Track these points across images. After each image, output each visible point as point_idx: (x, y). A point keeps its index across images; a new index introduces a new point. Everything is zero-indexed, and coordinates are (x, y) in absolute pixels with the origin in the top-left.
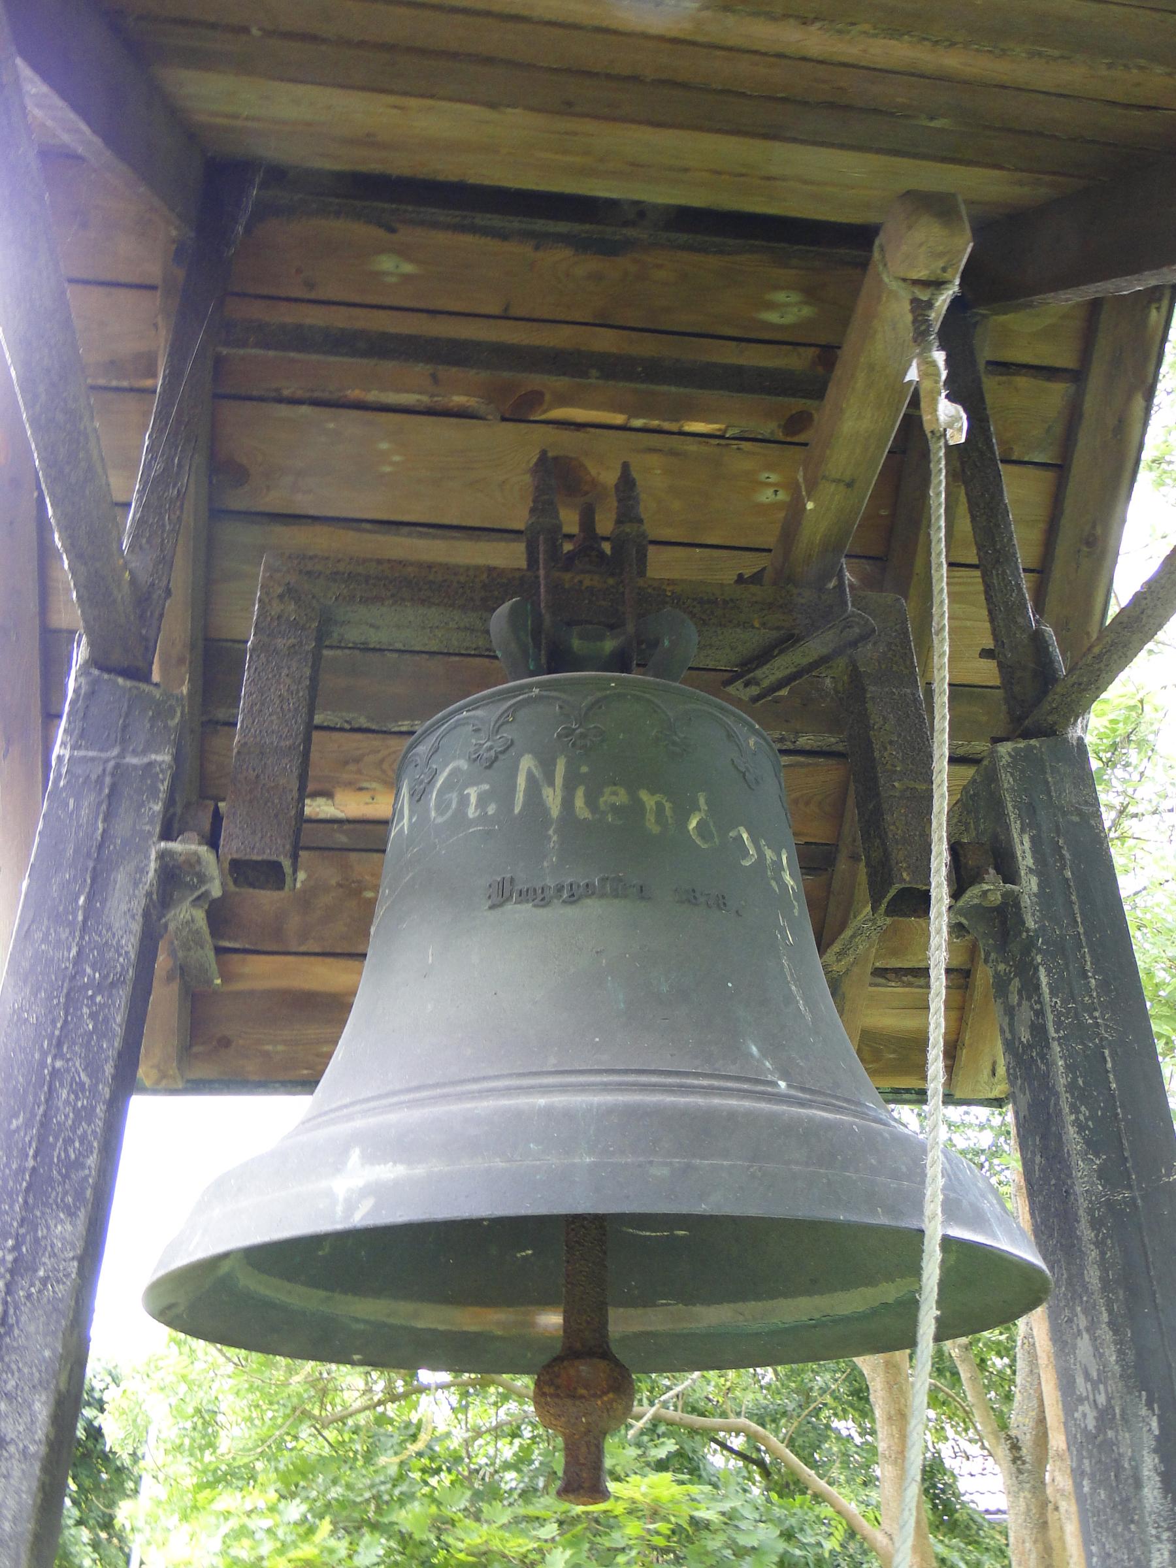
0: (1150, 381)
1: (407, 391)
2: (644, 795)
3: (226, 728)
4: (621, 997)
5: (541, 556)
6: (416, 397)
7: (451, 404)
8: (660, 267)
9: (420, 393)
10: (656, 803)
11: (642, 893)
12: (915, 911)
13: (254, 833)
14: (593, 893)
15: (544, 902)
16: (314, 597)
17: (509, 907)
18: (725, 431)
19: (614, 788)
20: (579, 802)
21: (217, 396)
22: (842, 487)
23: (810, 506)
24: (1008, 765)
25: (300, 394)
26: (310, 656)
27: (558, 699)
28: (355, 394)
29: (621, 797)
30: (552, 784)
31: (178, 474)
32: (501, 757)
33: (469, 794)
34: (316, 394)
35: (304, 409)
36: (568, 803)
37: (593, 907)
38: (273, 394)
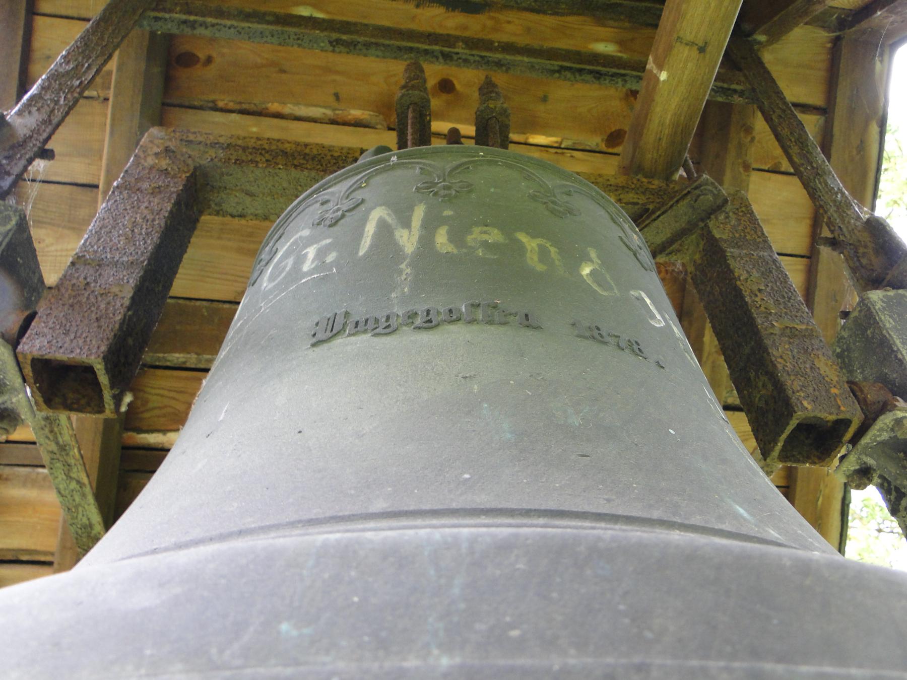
0: (881, 113)
1: (315, 106)
2: (523, 237)
3: (152, 370)
4: (506, 426)
6: (323, 110)
7: (350, 117)
8: (509, 22)
9: (325, 107)
10: (539, 246)
11: (528, 322)
12: (808, 458)
14: (458, 320)
15: (390, 330)
17: (339, 341)
18: (561, 143)
19: (485, 229)
20: (441, 238)
21: (164, 104)
22: (695, 53)
23: (663, 76)
25: (231, 106)
26: (174, 196)
27: (418, 163)
28: (275, 107)
29: (495, 236)
30: (407, 224)
31: (85, 72)
32: (347, 214)
33: (306, 254)
34: (244, 106)
35: (234, 116)
36: (426, 240)
37: (457, 334)
38: (211, 105)
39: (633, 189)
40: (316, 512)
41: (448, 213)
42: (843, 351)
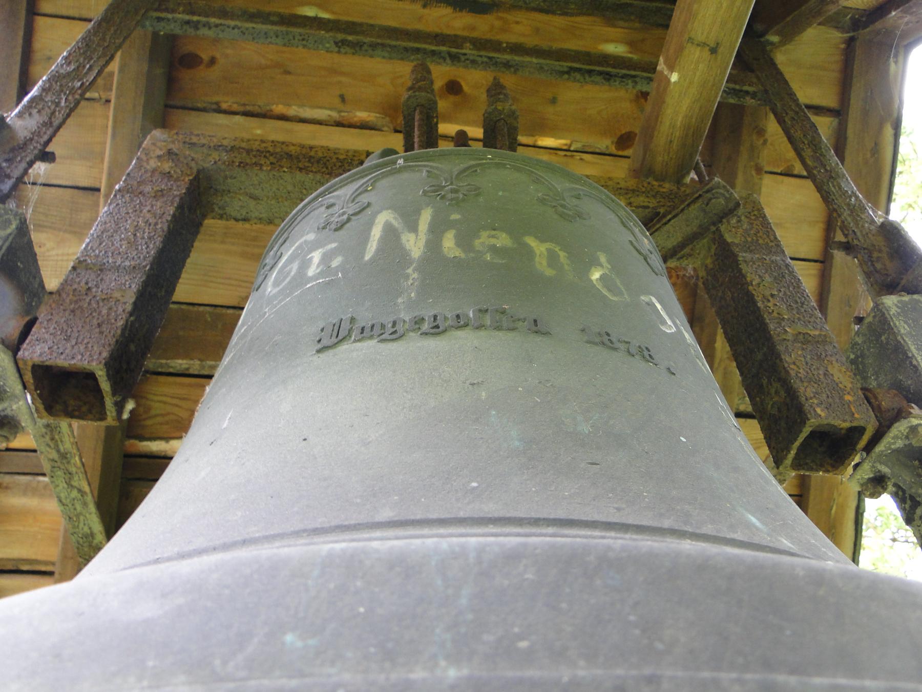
0: (895, 115)
1: (321, 108)
2: (531, 241)
3: (155, 377)
4: (514, 433)
5: (416, 124)
6: (328, 112)
7: (355, 119)
8: (517, 23)
9: (331, 109)
10: (548, 250)
11: (536, 327)
12: (822, 466)
13: (68, 339)
14: (466, 325)
15: (396, 336)
16: (193, 160)
17: (344, 347)
18: (570, 146)
19: (493, 233)
20: (449, 242)
21: (166, 106)
22: (706, 54)
23: (674, 77)
24: (898, 313)
25: (235, 107)
26: (177, 199)
27: (425, 166)
28: (279, 109)
29: (503, 240)
30: (414, 228)
31: (87, 73)
32: (353, 218)
33: (311, 258)
34: (248, 108)
35: (238, 118)
36: (433, 244)
37: (465, 340)
40: (321, 521)
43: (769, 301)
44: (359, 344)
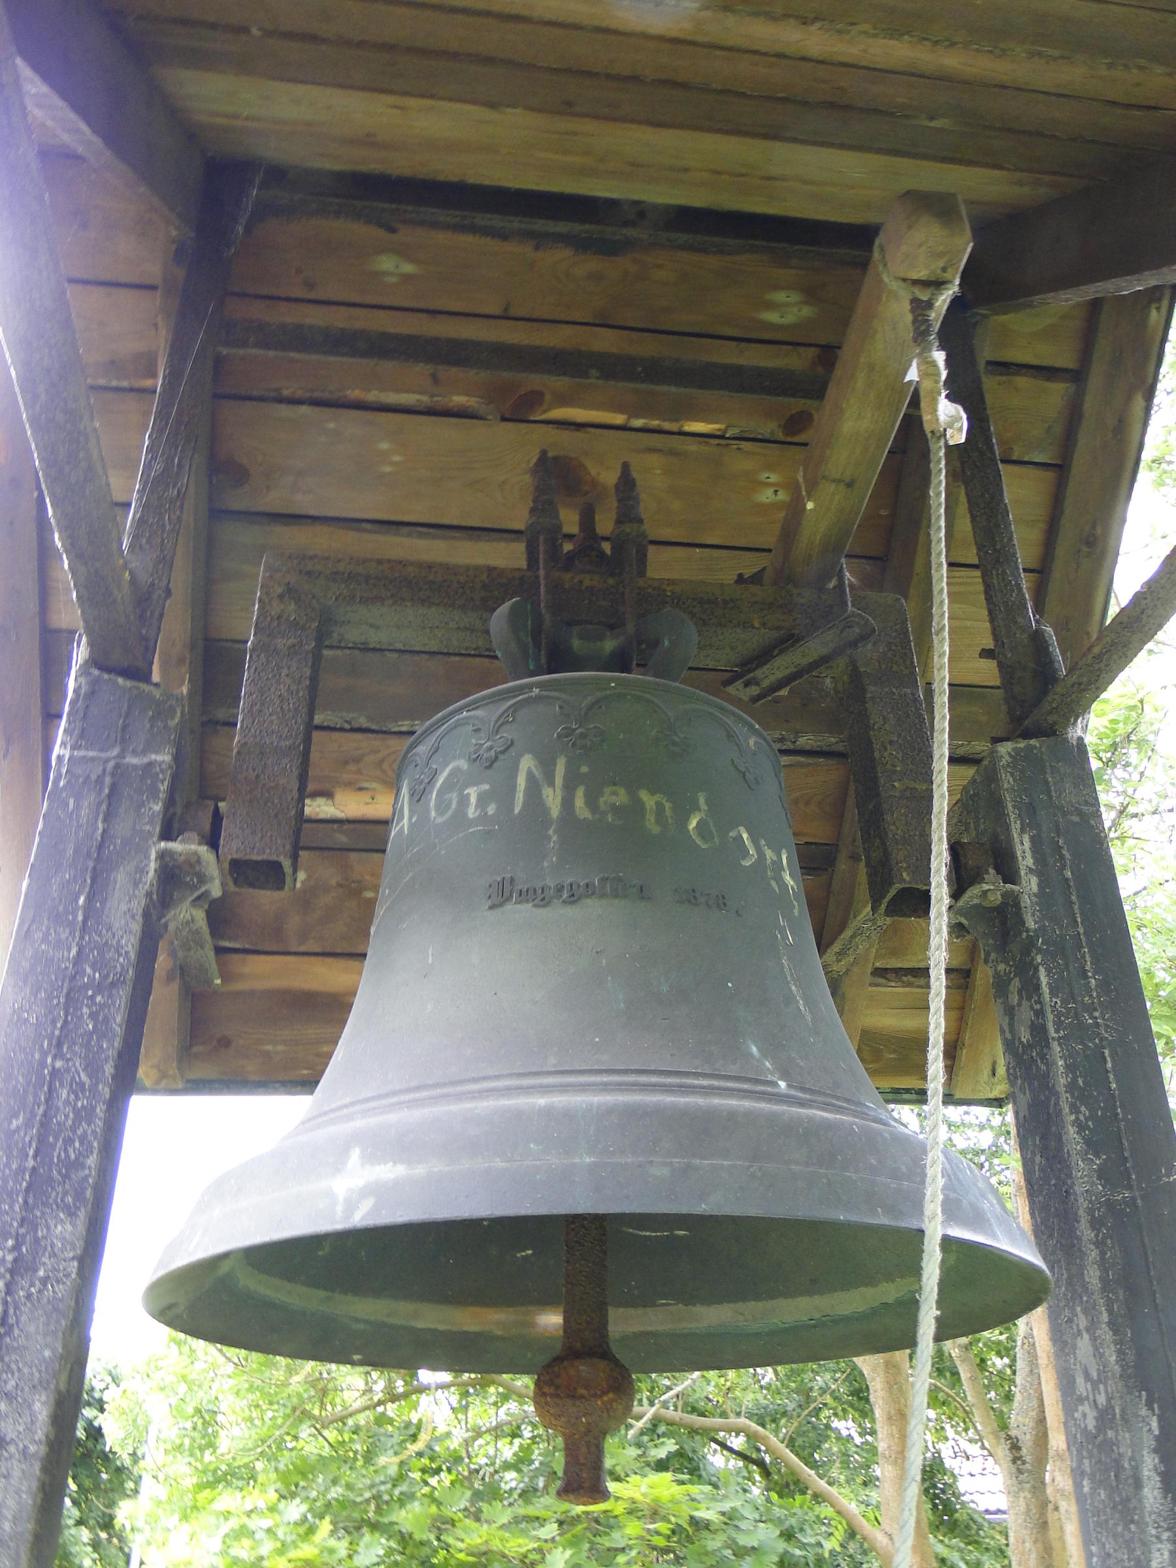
0: (1150, 381)
1: (407, 391)
2: (644, 795)
3: (226, 728)
4: (621, 997)
6: (416, 397)
7: (451, 404)
8: (660, 267)
9: (420, 393)
10: (656, 803)
11: (642, 893)
12: (915, 911)
13: (254, 833)
14: (593, 893)
15: (544, 902)
17: (509, 907)
18: (725, 431)
19: (614, 788)
20: (579, 802)
21: (217, 396)
22: (842, 487)
23: (810, 506)
24: (1008, 765)
25: (300, 394)
26: (310, 656)
27: (558, 699)
28: (355, 394)
29: (621, 797)
30: (552, 784)
31: (178, 474)
32: (501, 757)
33: (469, 794)
34: (316, 394)
35: (304, 409)
36: (568, 803)
37: (593, 907)
39: (781, 607)
40: (123, 279)
41: (584, 769)
42: (974, 795)
43: (886, 749)
44: (518, 906)
